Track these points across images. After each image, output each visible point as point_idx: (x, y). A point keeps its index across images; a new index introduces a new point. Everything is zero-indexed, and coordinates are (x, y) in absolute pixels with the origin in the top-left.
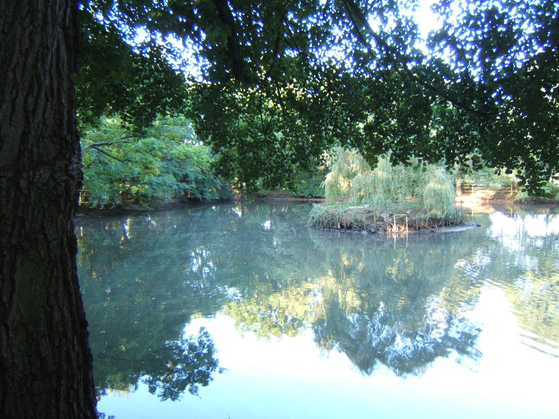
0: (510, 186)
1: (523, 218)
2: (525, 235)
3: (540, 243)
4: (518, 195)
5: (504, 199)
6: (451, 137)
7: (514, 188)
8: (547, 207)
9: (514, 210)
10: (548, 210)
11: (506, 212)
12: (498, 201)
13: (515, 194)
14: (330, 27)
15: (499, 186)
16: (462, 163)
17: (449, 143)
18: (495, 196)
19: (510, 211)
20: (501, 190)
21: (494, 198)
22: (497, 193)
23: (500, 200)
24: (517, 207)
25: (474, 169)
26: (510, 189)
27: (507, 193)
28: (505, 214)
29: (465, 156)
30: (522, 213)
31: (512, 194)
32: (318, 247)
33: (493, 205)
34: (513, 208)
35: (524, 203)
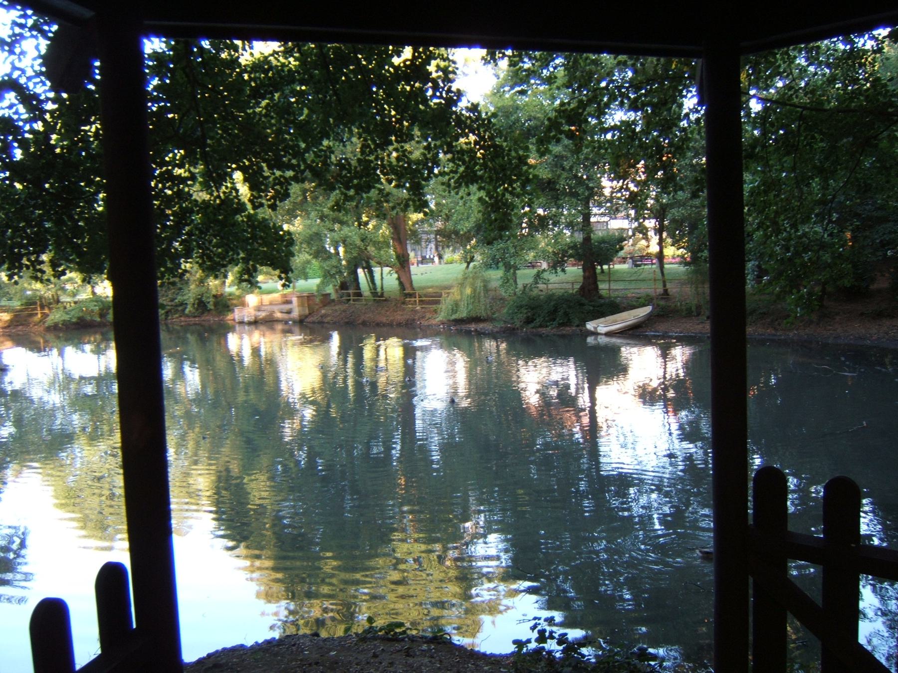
0: (35, 303)
1: (61, 354)
2: (69, 378)
3: (89, 389)
4: (51, 317)
5: (27, 325)
6: (16, 230)
7: (42, 307)
8: (95, 333)
9: (46, 342)
10: (98, 337)
11: (35, 347)
12: (241, 312)
13: (45, 316)
14: (384, 190)
15: (16, 304)
16: (34, 267)
17: (11, 238)
18: (11, 321)
19: (39, 343)
20: (21, 311)
21: (11, 324)
22: (16, 316)
23: (20, 327)
24: (50, 337)
25: (55, 276)
26: (35, 309)
27: (31, 315)
28: (31, 350)
29: (38, 256)
30: (59, 345)
31: (39, 316)
32: (256, 351)
33: (9, 336)
34: (44, 338)
35: (60, 330)
